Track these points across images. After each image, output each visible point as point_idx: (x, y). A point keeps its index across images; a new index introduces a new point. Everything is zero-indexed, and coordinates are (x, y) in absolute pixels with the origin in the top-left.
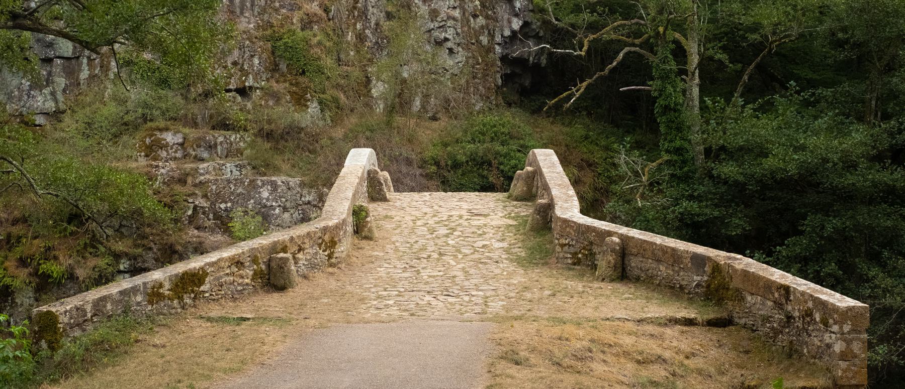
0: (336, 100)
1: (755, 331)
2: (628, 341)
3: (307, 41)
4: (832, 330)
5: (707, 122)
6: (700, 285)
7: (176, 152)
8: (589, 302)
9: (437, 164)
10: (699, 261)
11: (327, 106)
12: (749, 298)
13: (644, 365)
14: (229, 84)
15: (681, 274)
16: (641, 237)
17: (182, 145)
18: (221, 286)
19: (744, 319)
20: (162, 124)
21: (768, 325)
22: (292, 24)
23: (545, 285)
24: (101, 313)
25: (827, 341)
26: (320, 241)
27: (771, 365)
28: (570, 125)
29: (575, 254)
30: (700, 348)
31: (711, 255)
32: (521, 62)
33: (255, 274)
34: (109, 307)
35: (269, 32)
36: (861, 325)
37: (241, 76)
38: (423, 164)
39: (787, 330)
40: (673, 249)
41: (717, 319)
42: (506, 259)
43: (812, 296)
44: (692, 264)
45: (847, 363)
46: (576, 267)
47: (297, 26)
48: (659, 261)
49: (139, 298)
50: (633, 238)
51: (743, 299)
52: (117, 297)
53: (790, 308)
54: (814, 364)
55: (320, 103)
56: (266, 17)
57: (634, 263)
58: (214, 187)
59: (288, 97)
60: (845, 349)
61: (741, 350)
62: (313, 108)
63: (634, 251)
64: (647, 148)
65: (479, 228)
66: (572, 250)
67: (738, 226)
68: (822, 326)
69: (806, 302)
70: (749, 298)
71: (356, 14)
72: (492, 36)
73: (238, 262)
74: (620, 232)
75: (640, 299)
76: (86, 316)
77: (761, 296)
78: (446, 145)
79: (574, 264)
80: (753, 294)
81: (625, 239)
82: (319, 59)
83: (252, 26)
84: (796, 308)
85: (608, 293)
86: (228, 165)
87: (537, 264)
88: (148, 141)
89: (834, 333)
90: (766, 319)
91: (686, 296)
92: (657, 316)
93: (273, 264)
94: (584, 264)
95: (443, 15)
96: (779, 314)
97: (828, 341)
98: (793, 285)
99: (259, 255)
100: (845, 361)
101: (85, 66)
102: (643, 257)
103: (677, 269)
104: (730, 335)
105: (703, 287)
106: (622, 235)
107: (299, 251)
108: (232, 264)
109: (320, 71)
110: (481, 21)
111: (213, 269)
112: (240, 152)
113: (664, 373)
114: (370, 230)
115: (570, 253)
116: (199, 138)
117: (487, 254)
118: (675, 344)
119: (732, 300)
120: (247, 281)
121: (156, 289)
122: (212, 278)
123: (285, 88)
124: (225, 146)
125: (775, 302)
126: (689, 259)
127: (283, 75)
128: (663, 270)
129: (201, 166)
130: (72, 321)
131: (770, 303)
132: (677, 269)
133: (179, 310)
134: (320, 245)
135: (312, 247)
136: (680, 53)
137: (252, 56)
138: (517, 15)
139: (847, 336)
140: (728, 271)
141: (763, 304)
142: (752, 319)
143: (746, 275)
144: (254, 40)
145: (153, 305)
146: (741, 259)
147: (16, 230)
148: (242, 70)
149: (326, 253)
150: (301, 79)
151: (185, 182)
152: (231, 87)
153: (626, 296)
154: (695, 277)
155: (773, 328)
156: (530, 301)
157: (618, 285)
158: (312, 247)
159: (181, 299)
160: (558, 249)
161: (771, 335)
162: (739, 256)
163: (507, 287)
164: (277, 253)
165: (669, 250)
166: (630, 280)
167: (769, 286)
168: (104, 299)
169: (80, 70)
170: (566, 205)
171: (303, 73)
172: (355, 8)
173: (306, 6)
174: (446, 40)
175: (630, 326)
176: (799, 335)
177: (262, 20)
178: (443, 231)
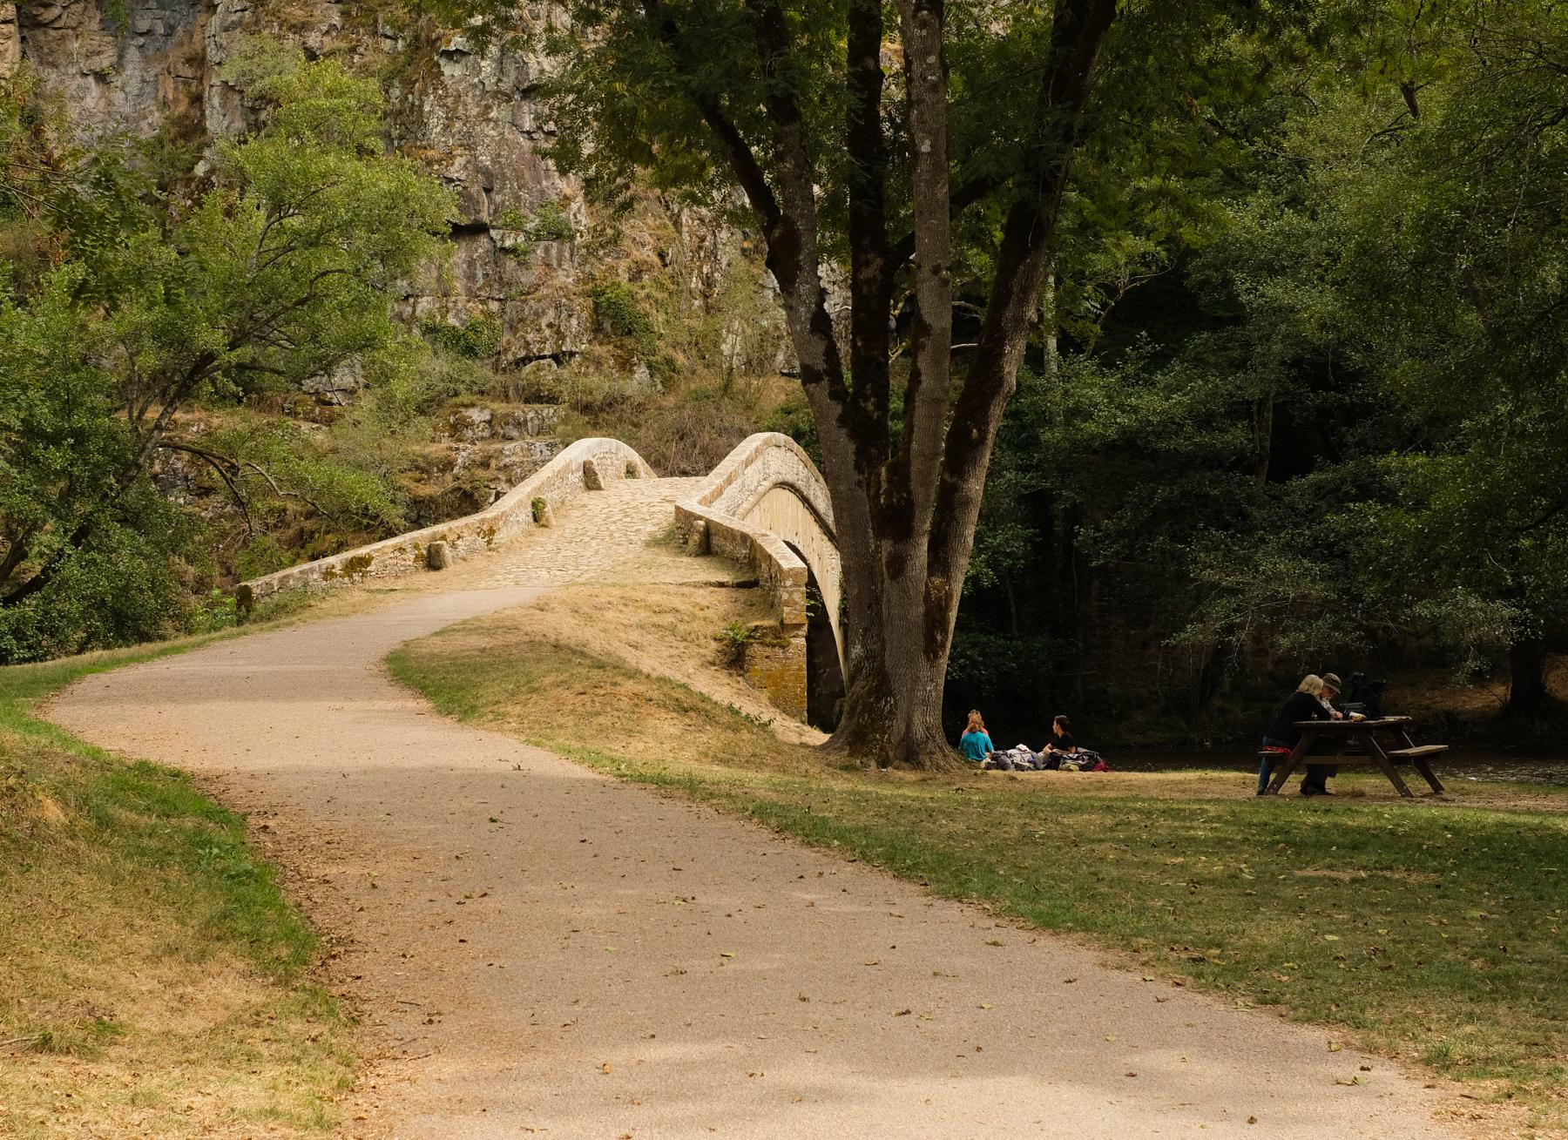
0: (669, 362)
3: (632, 295)
7: (483, 430)
11: (658, 370)
14: (543, 349)
17: (489, 422)
20: (465, 398)
22: (618, 275)
33: (417, 557)
34: (291, 582)
35: (590, 286)
37: (558, 340)
47: (624, 277)
49: (315, 576)
52: (298, 575)
55: (649, 366)
56: (587, 268)
57: (715, 541)
58: (519, 471)
59: (612, 362)
62: (641, 373)
67: (1067, 499)
71: (702, 254)
82: (647, 315)
83: (570, 280)
86: (538, 444)
88: (452, 419)
93: (432, 550)
109: (648, 329)
112: (552, 429)
114: (547, 520)
116: (507, 415)
123: (608, 351)
124: (536, 422)
127: (607, 336)
129: (507, 447)
134: (478, 534)
137: (570, 316)
144: (572, 297)
147: (309, 525)
148: (558, 332)
151: (488, 466)
152: (546, 353)
157: (700, 560)
159: (351, 576)
168: (287, 577)
171: (630, 333)
172: (700, 248)
173: (635, 252)
177: (583, 272)
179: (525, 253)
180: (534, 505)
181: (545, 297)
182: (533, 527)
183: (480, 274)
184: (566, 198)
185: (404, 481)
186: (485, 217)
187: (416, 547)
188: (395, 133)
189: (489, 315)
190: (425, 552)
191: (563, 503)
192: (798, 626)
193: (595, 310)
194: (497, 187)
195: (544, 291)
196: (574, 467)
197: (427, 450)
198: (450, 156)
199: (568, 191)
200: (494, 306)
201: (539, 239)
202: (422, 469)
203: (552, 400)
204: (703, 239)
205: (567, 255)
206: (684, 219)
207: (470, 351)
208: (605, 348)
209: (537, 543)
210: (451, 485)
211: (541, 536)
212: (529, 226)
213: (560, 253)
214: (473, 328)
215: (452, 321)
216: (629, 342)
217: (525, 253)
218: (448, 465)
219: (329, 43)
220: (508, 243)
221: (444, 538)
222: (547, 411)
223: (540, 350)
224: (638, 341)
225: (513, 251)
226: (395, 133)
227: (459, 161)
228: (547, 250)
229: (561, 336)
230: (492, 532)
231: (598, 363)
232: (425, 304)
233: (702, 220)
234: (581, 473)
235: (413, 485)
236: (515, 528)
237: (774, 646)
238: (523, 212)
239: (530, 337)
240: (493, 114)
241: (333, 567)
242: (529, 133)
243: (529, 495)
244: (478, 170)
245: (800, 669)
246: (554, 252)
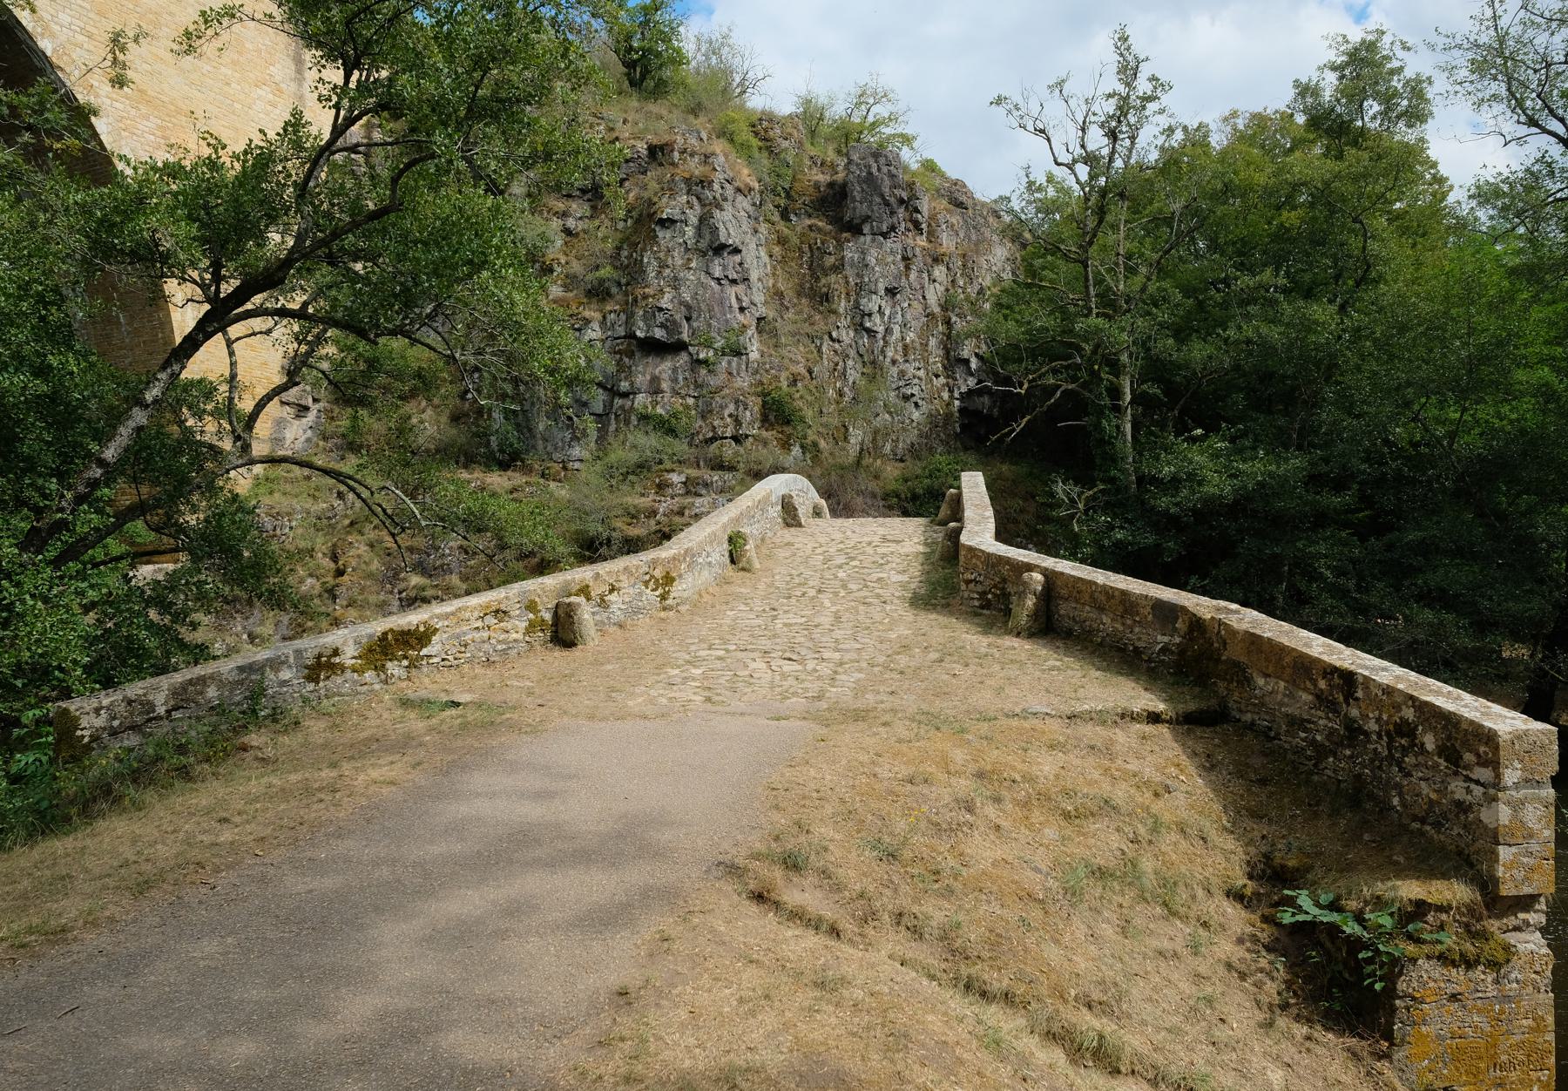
0: (815, 444)
1: (1274, 738)
2: (1046, 766)
4: (1474, 777)
5: (1141, 454)
6: (1168, 650)
8: (990, 675)
9: (898, 496)
10: (1166, 612)
12: (1261, 681)
13: (1077, 821)
15: (1137, 630)
16: (1073, 573)
17: (684, 483)
18: (465, 646)
19: (1249, 715)
20: (668, 465)
21: (1303, 735)
23: (934, 643)
24: (193, 705)
25: (1457, 796)
26: (647, 577)
27: (1316, 815)
28: (1016, 464)
29: (983, 594)
30: (1177, 772)
31: (1186, 604)
32: (977, 414)
35: (759, 389)
36: (1541, 768)
38: (886, 497)
39: (1348, 752)
40: (1124, 593)
41: (1201, 712)
42: (898, 598)
43: (1412, 697)
44: (1154, 616)
45: (1514, 849)
46: (985, 612)
47: (784, 384)
48: (1101, 609)
49: (286, 674)
50: (1062, 574)
51: (1249, 680)
52: (234, 676)
53: (1354, 712)
54: (1422, 834)
55: (802, 447)
56: (758, 377)
57: (1064, 609)
60: (1510, 821)
61: (1253, 777)
63: (1064, 592)
64: (1084, 481)
65: (884, 556)
66: (980, 588)
68: (1441, 761)
69: (1398, 708)
70: (1261, 681)
72: (951, 391)
73: (497, 611)
74: (1043, 565)
75: (1073, 669)
76: (154, 711)
77: (1287, 682)
78: (906, 481)
79: (982, 607)
80: (1269, 676)
81: (1050, 577)
82: (801, 410)
84: (1371, 715)
85: (1023, 657)
87: (935, 606)
88: (657, 481)
89: (1477, 782)
90: (1296, 723)
91: (1145, 665)
92: (1100, 707)
93: (560, 612)
94: (995, 609)
95: (910, 375)
96: (1328, 718)
97: (1460, 795)
98: (1360, 671)
99: (537, 599)
100: (1510, 845)
101: (613, 422)
102: (1077, 601)
103: (1129, 622)
104: (1226, 743)
105: (1172, 653)
106: (1046, 569)
107: (612, 590)
108: (486, 614)
109: (802, 420)
110: (942, 380)
111: (446, 623)
113: (1116, 841)
115: (978, 593)
117: (877, 591)
118: (1133, 766)
119: (1225, 679)
120: (515, 636)
121: (324, 659)
122: (445, 636)
125: (1318, 697)
126: (1149, 609)
128: (1108, 623)
130: (116, 723)
131: (1306, 697)
132: (1129, 622)
133: (377, 687)
134: (646, 583)
135: (633, 586)
136: (1115, 393)
138: (972, 374)
139: (1514, 793)
140: (1219, 632)
141: (1291, 696)
142: (1267, 718)
143: (1254, 641)
145: (317, 683)
146: (1237, 612)
149: (657, 593)
150: (785, 429)
153: (1051, 663)
154: (1159, 637)
155: (1313, 742)
156: (902, 673)
158: (633, 586)
160: (963, 587)
161: (1309, 753)
162: (1234, 606)
163: (879, 646)
164: (569, 595)
165: (1116, 593)
166: (1059, 634)
167: (1304, 667)
169: (609, 424)
170: (976, 528)
174: (913, 395)
175: (1055, 728)
176: (1380, 768)
178: (841, 560)
179: (714, 364)
180: (730, 540)
181: (727, 395)
182: (730, 571)
183: (681, 378)
184: (744, 326)
185: (618, 524)
186: (685, 337)
187: (531, 607)
188: (623, 281)
189: (687, 407)
190: (548, 616)
191: (763, 540)
192: (1526, 902)
193: (763, 406)
194: (694, 316)
195: (726, 391)
196: (773, 499)
197: (636, 502)
198: (662, 291)
199: (746, 322)
200: (691, 401)
201: (724, 354)
202: (633, 516)
203: (732, 468)
204: (837, 364)
205: (744, 367)
206: (824, 349)
207: (671, 432)
208: (770, 433)
209: (737, 597)
210: (654, 528)
211: (741, 584)
212: (717, 345)
213: (739, 365)
214: (675, 415)
215: (659, 410)
216: (788, 430)
217: (714, 364)
218: (654, 513)
219: (581, 225)
220: (702, 356)
221: (584, 591)
222: (728, 476)
223: (723, 433)
224: (794, 428)
225: (705, 362)
226: (623, 281)
227: (667, 297)
228: (729, 363)
229: (738, 422)
230: (669, 580)
231: (765, 443)
232: (641, 400)
233: (835, 351)
234: (780, 507)
235: (625, 527)
236: (705, 573)
237: (1470, 964)
238: (712, 334)
239: (716, 423)
240: (693, 265)
241: (336, 652)
242: (718, 279)
243: (725, 527)
244: (681, 303)
245: (1538, 1029)
246: (734, 364)
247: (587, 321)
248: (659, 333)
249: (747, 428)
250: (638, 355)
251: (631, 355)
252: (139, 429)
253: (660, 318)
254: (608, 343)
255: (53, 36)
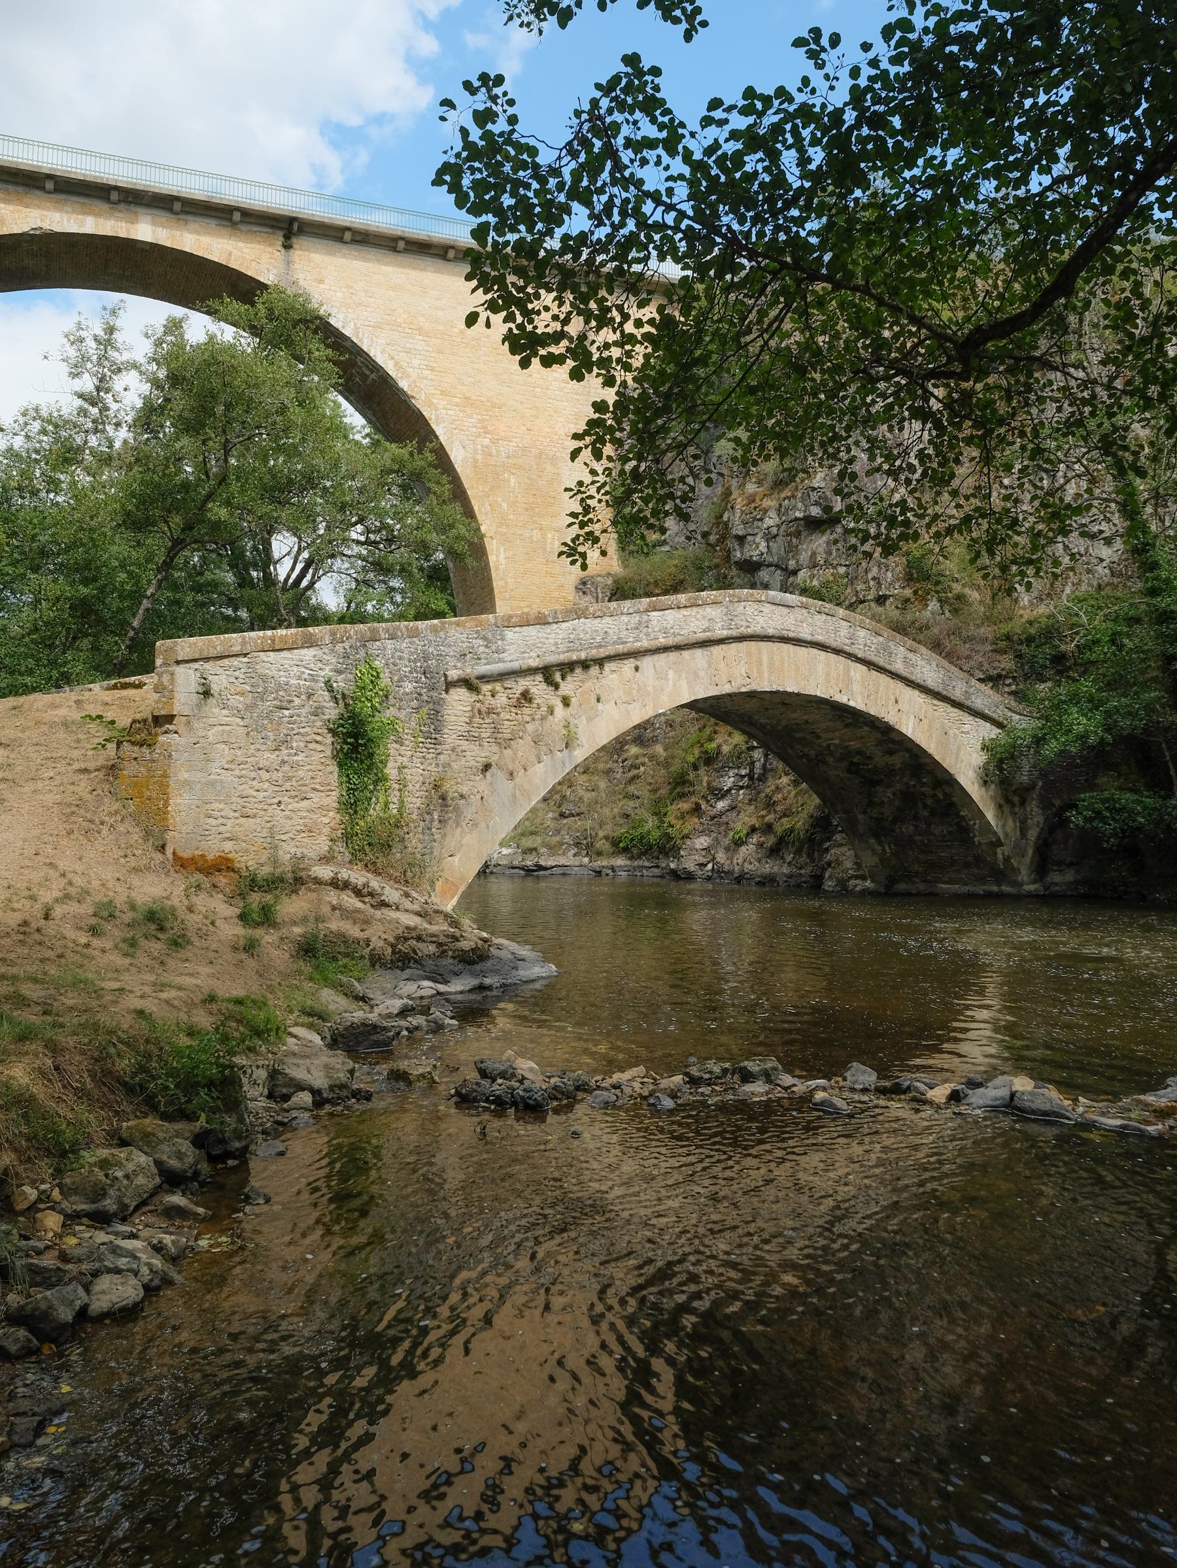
55: (940, 601)
215: (815, 583)
247: (766, 511)
248: (815, 511)
249: (888, 589)
250: (804, 534)
251: (798, 534)
252: (147, 610)
253: (814, 496)
254: (783, 527)
255: (408, 376)
